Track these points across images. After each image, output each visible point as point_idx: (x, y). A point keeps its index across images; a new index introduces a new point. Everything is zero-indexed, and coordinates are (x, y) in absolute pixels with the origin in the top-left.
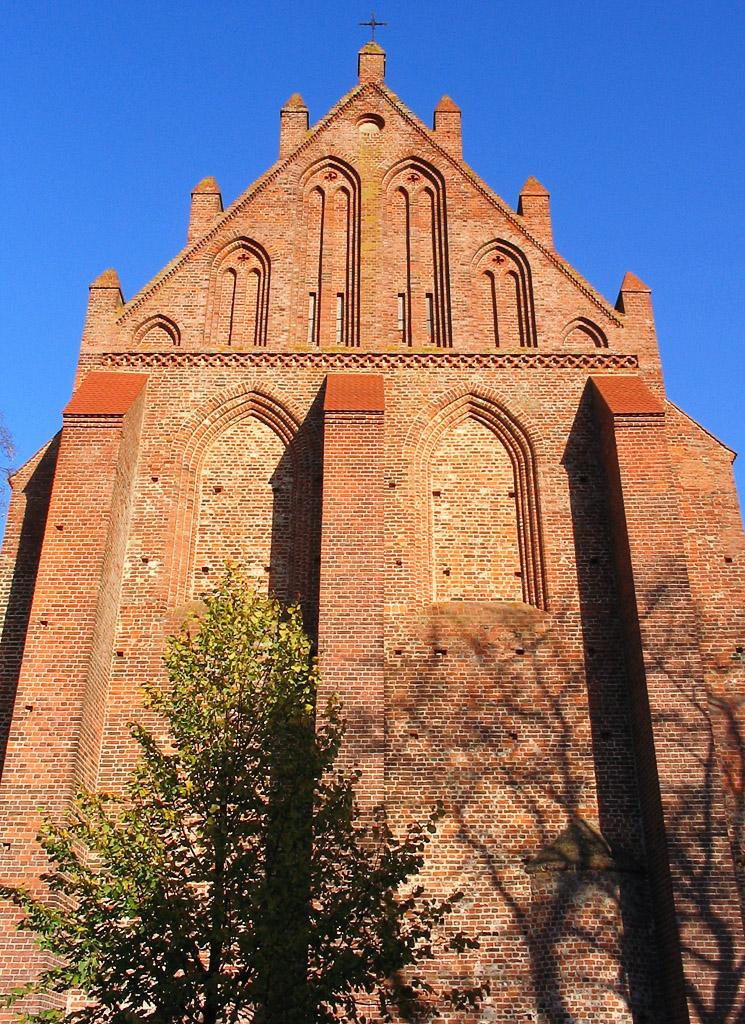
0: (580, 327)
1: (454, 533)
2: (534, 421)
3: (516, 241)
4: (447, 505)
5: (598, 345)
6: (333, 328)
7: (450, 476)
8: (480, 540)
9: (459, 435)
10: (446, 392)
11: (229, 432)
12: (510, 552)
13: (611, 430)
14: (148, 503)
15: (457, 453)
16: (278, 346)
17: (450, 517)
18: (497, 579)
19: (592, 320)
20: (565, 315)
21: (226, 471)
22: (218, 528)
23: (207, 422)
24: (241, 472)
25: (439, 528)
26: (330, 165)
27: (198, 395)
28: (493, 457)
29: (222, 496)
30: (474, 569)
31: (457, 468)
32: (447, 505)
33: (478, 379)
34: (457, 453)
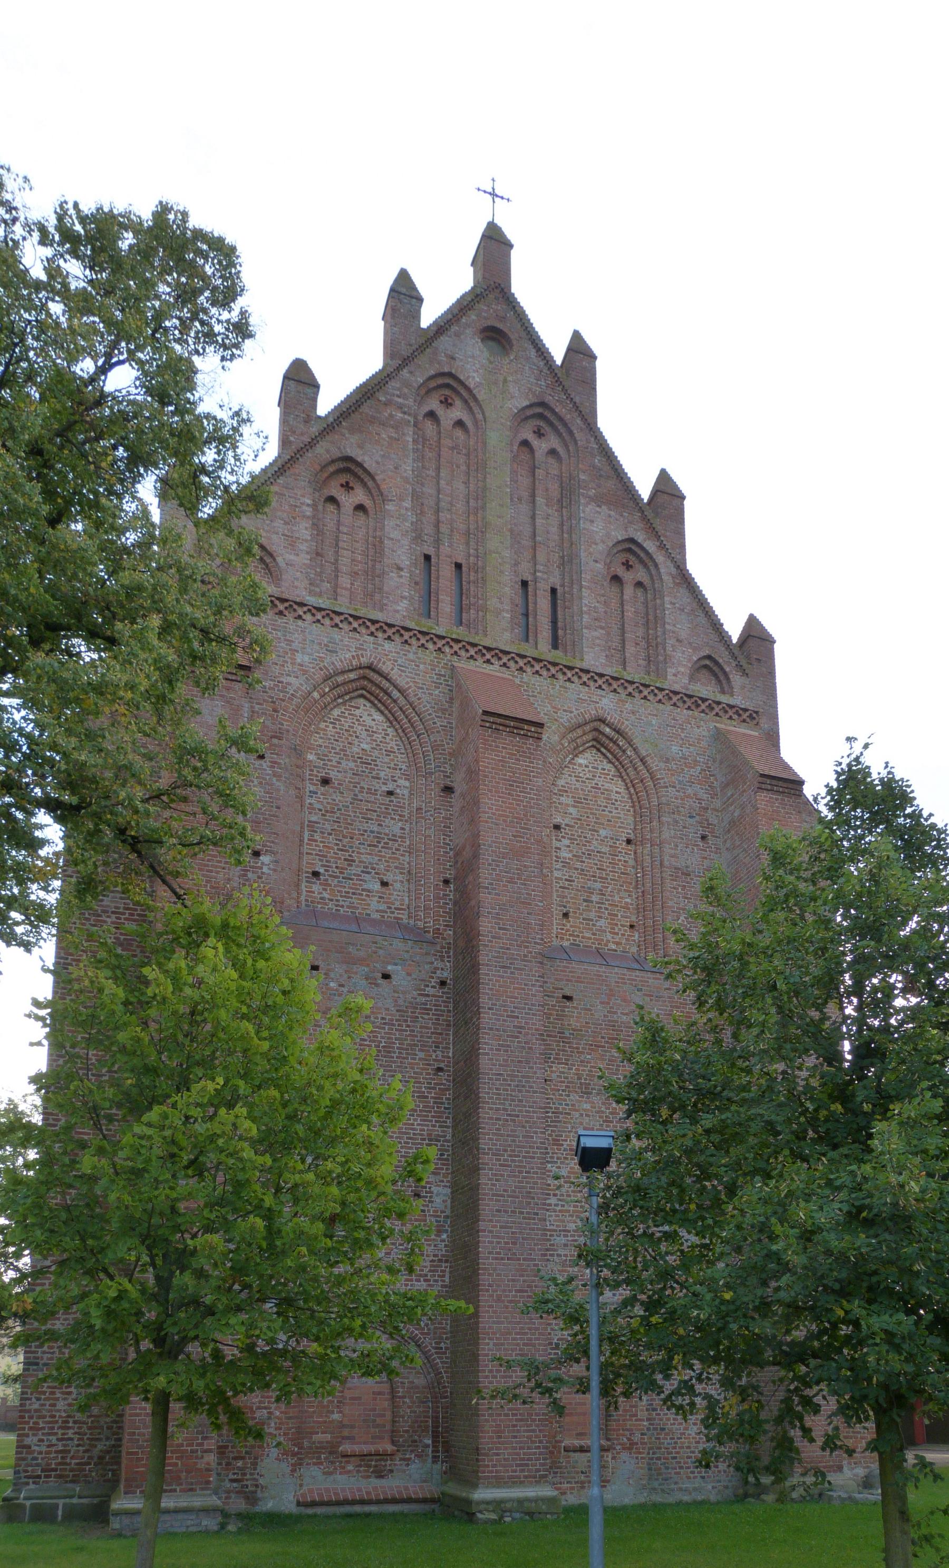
0: (705, 666)
1: (575, 874)
2: (662, 765)
3: (650, 546)
4: (567, 842)
5: (723, 692)
6: (446, 604)
7: (571, 810)
8: (598, 885)
9: (580, 765)
10: (576, 712)
11: (336, 712)
12: (627, 903)
13: (56, 964)
14: (256, 783)
15: (578, 785)
16: (397, 615)
17: (570, 855)
18: (23, 1417)
19: (721, 661)
20: (695, 649)
21: (334, 760)
22: (328, 827)
23: (316, 695)
24: (352, 765)
25: (559, 865)
26: (448, 386)
27: (306, 658)
28: (614, 796)
29: (331, 790)
30: (592, 915)
31: (577, 803)
32: (567, 842)
33: (607, 703)
34: (578, 785)
